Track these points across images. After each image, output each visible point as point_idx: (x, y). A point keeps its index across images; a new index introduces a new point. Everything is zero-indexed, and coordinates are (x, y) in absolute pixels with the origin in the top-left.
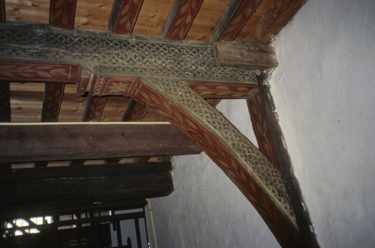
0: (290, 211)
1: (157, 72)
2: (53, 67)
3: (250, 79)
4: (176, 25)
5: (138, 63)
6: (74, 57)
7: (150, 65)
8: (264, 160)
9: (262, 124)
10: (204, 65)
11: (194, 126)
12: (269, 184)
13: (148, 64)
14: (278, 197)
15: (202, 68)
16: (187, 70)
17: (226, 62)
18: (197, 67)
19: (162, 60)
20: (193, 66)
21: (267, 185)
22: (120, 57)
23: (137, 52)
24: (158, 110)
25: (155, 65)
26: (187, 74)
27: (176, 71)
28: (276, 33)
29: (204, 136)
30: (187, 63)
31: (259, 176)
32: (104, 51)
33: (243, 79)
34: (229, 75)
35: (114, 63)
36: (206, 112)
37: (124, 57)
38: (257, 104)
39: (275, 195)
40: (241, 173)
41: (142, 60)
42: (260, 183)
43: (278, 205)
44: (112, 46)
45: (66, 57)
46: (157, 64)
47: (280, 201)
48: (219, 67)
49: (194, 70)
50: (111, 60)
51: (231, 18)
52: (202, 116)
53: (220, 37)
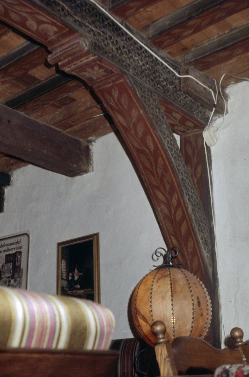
0: (210, 261)
1: (138, 73)
2: (50, 22)
3: (202, 117)
4: (172, 32)
5: (124, 55)
6: (75, 21)
7: (133, 63)
8: (200, 205)
9: (196, 168)
10: (173, 85)
11: (152, 146)
12: (200, 230)
13: (131, 60)
14: (204, 245)
15: (171, 87)
16: (159, 83)
17: (192, 91)
18: (167, 84)
19: (143, 62)
20: (164, 81)
21: (199, 230)
22: (112, 41)
23: (125, 42)
24: (116, 113)
25: (137, 64)
26: (159, 88)
27: (152, 80)
28: (238, 81)
29: (156, 161)
30: (161, 75)
31: (195, 219)
32: (100, 28)
33: (197, 114)
34: (189, 105)
35: (105, 45)
36: (168, 137)
37: (115, 43)
38: (195, 146)
39: (202, 242)
40: (178, 212)
41: (128, 53)
42: (194, 226)
43: (203, 252)
44: (106, 25)
45: (69, 18)
46: (139, 65)
47: (205, 249)
48: (182, 93)
49: (164, 85)
50: (104, 41)
51: (218, 49)
52: (165, 138)
53: (193, 61)
